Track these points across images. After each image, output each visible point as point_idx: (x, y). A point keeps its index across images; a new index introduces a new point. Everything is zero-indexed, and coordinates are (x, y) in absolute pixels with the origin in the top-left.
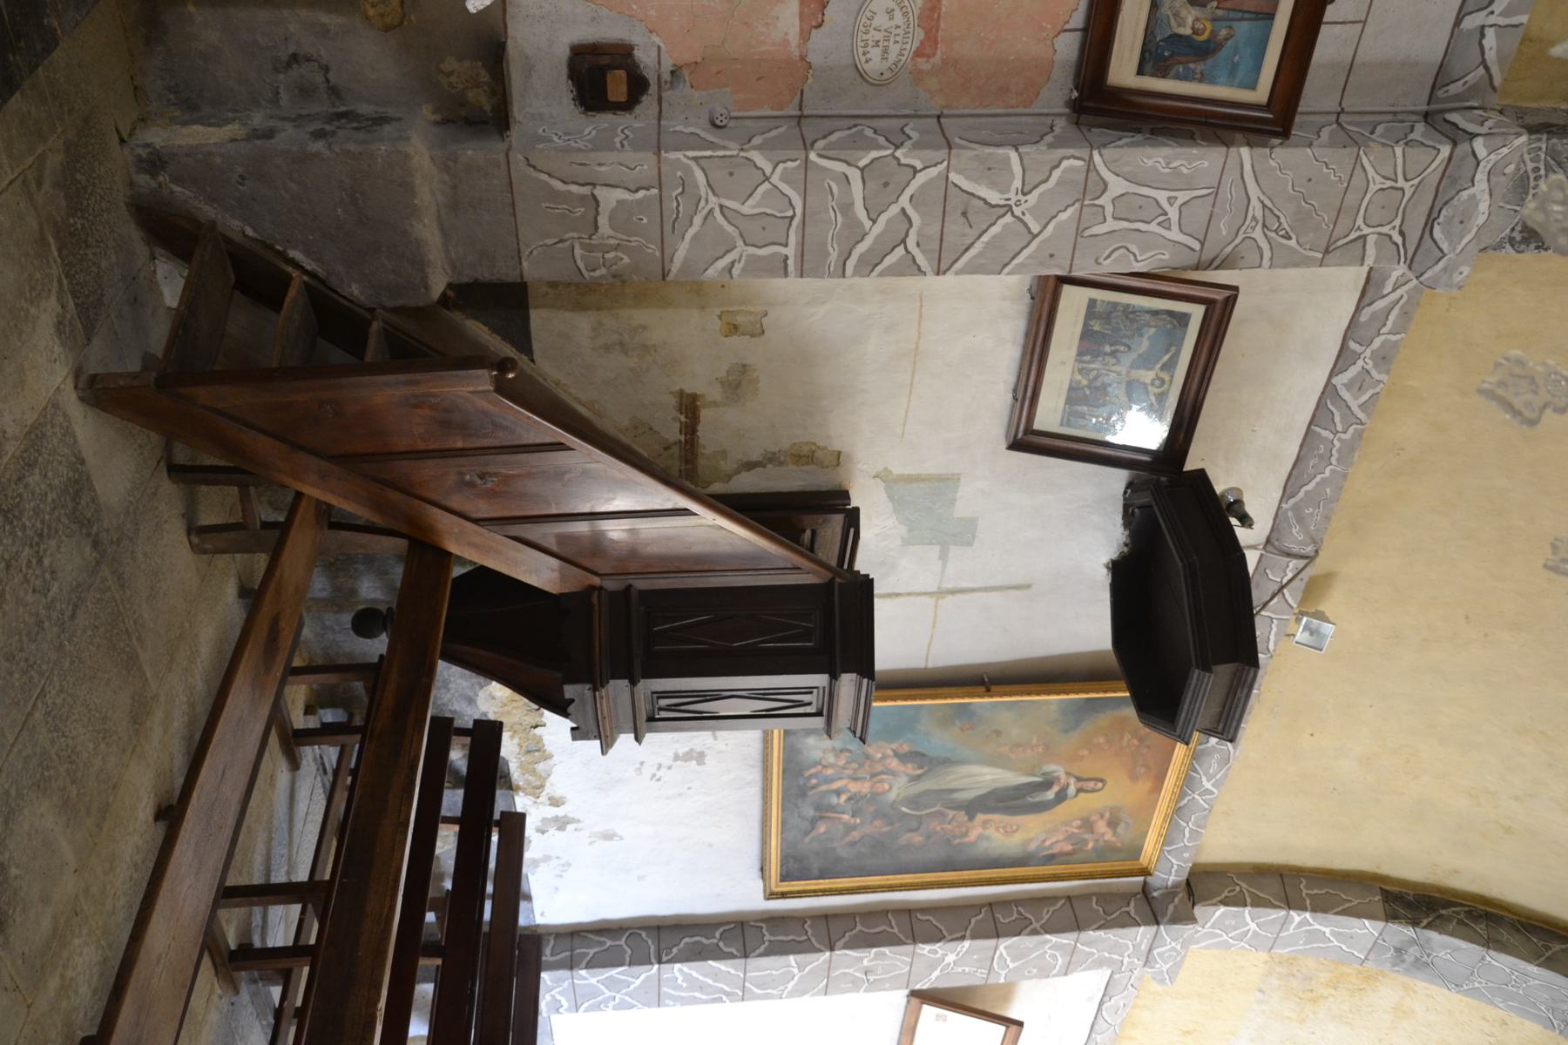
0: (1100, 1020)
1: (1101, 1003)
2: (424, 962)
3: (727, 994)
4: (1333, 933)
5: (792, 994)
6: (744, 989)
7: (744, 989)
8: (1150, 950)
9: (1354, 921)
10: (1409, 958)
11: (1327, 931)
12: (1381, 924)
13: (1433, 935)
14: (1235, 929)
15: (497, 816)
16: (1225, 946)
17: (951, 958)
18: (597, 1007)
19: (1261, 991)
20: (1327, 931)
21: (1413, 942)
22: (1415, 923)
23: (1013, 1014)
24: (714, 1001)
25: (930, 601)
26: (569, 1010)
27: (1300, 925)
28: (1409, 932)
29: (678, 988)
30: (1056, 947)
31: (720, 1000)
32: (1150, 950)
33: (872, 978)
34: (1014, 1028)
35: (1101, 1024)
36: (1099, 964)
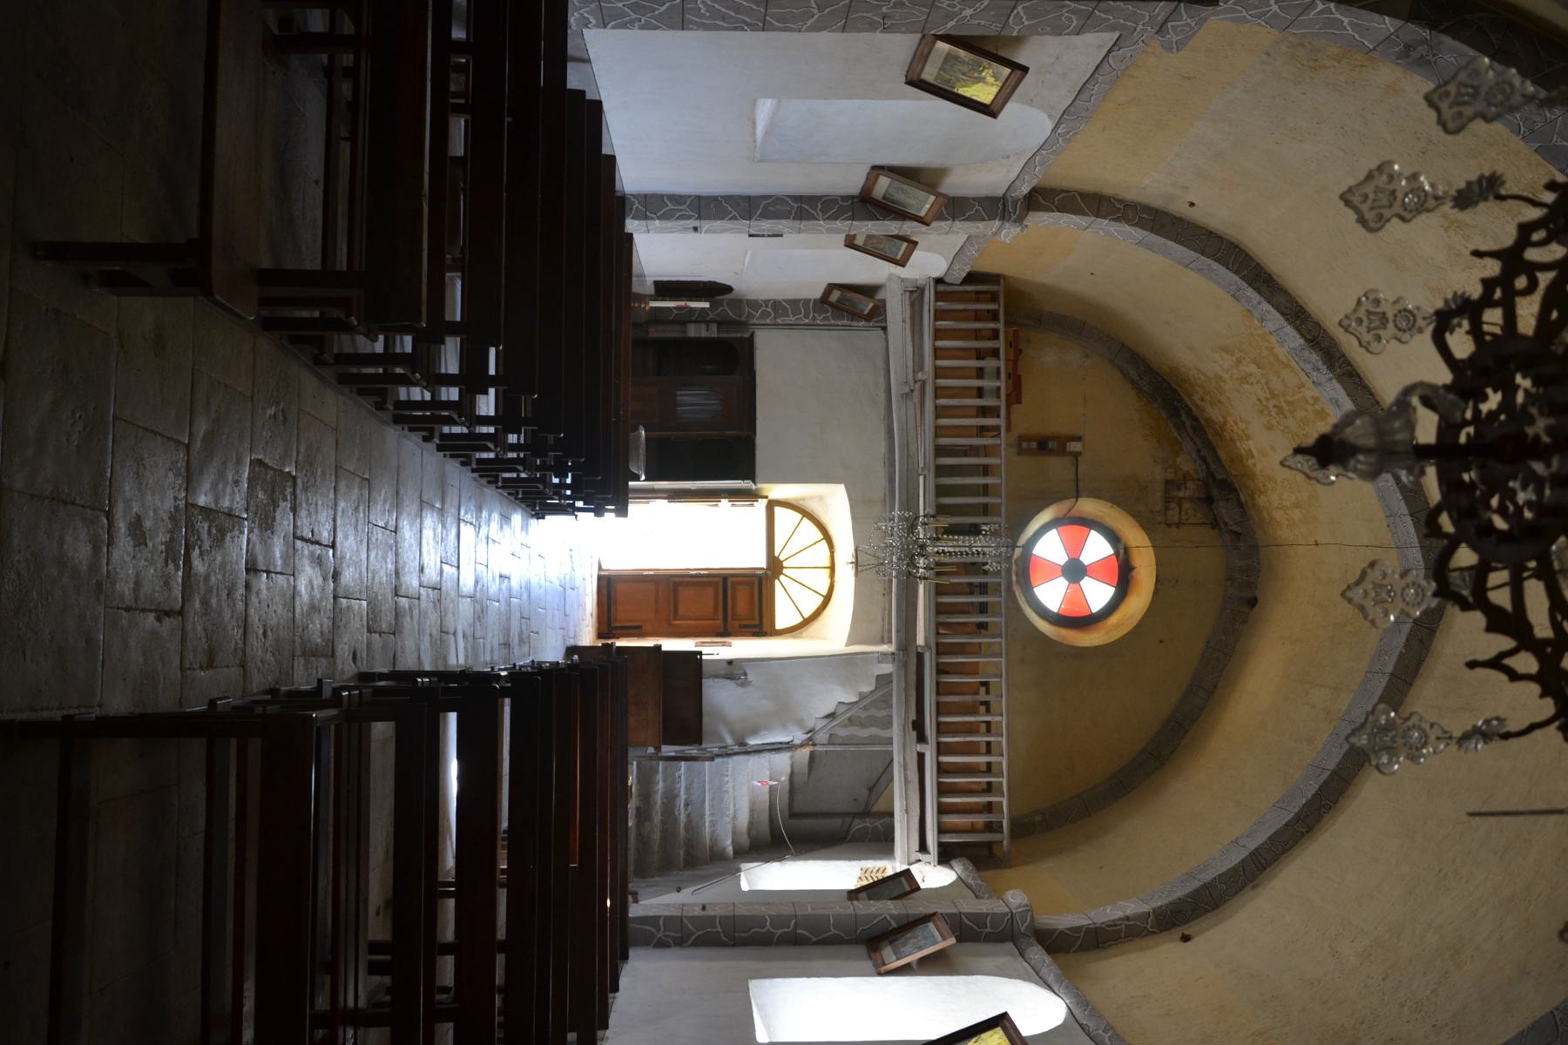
0: (1105, 65)
1: (1109, 51)
2: (444, 398)
3: (748, 25)
4: (1351, 23)
5: (810, 29)
6: (764, 21)
7: (764, 21)
8: (1165, 22)
9: (1376, 16)
10: (1414, 55)
11: (1346, 21)
12: (1399, 23)
13: (1447, 40)
14: (1257, 7)
15: (492, 391)
16: (1243, 20)
17: (968, 12)
18: (624, 26)
19: (1268, 54)
20: (1346, 21)
21: (1424, 41)
22: (1433, 26)
23: (1021, 59)
24: (735, 29)
25: (828, 564)
26: (597, 26)
27: (1321, 12)
28: (1426, 33)
29: (702, 16)
30: (1073, 11)
31: (742, 29)
32: (1165, 22)
33: (889, 22)
34: (1019, 73)
35: (1105, 66)
36: (1112, 28)
